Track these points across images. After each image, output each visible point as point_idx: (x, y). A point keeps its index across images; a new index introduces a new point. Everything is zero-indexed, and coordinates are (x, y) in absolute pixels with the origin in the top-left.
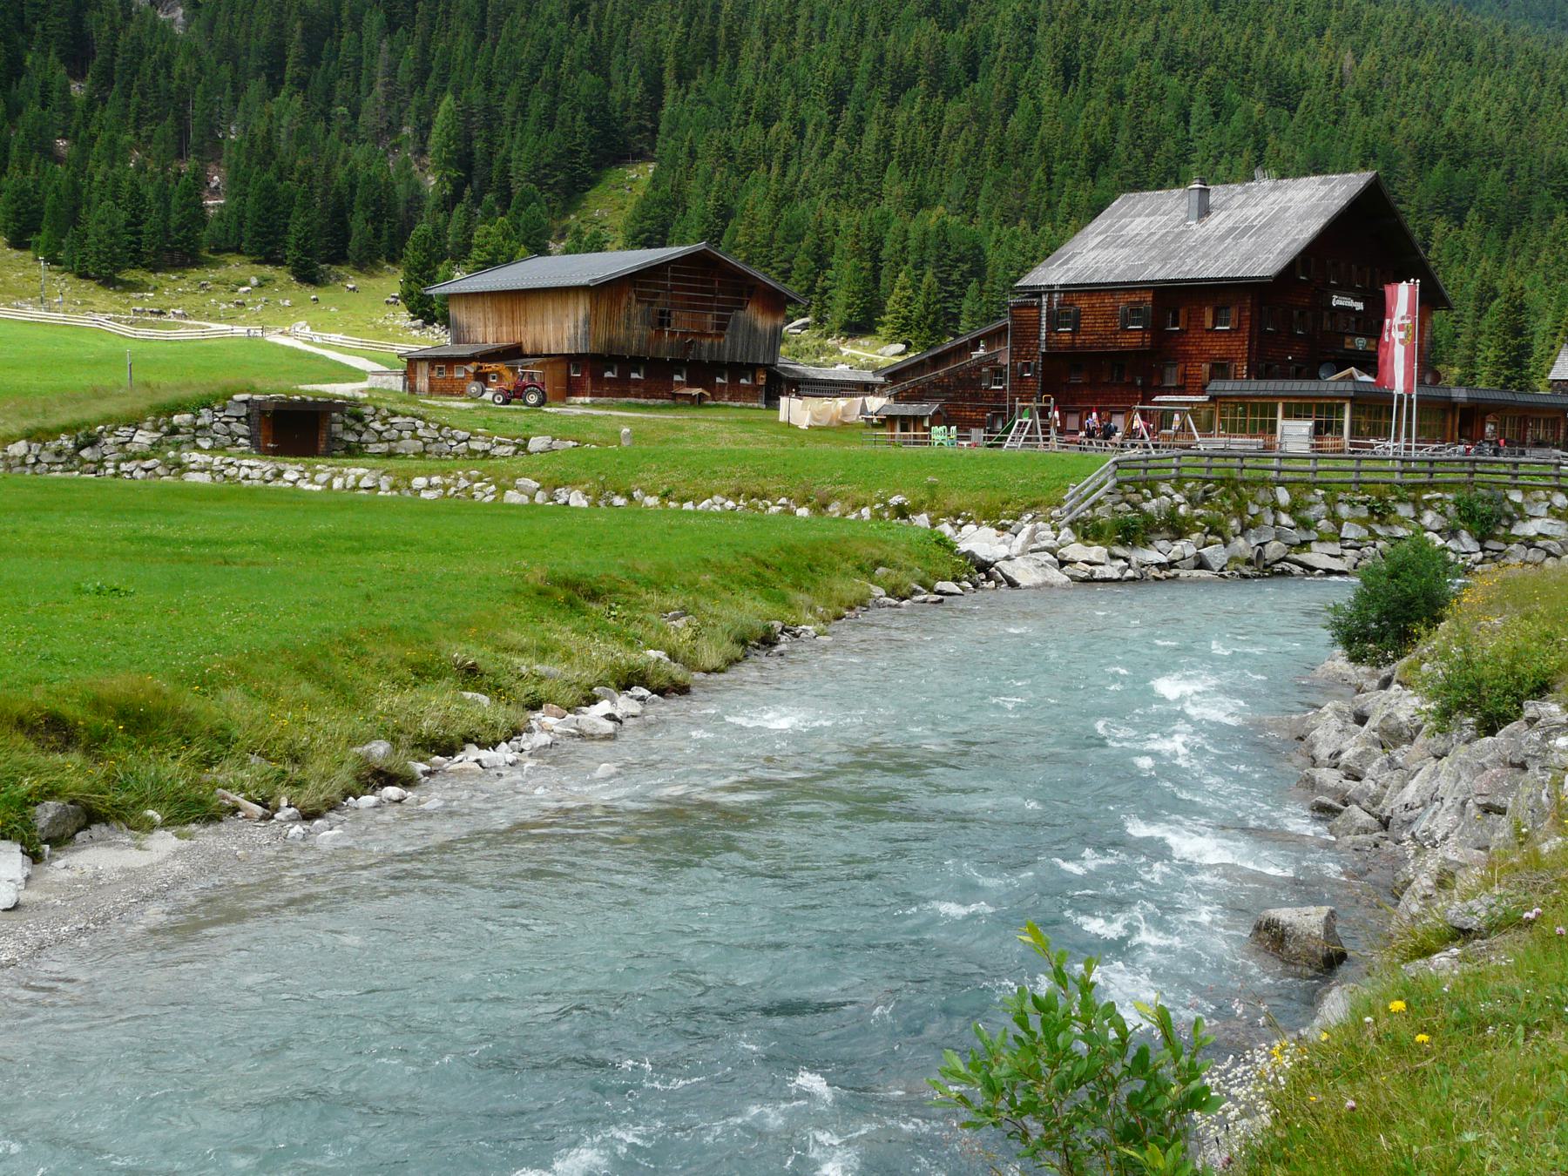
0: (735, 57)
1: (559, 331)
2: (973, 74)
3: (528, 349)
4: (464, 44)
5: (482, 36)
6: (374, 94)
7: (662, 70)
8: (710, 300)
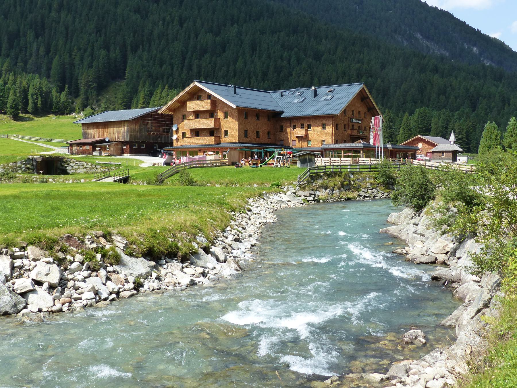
0: (150, 46)
1: (119, 133)
2: (224, 51)
3: (107, 140)
4: (61, 42)
5: (67, 40)
6: (32, 59)
7: (126, 51)
8: (164, 124)
